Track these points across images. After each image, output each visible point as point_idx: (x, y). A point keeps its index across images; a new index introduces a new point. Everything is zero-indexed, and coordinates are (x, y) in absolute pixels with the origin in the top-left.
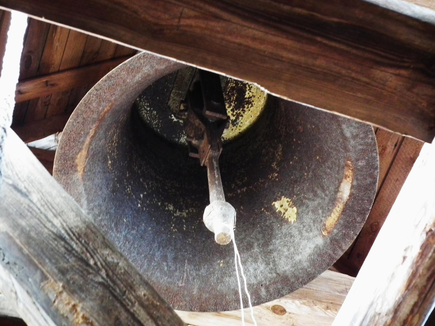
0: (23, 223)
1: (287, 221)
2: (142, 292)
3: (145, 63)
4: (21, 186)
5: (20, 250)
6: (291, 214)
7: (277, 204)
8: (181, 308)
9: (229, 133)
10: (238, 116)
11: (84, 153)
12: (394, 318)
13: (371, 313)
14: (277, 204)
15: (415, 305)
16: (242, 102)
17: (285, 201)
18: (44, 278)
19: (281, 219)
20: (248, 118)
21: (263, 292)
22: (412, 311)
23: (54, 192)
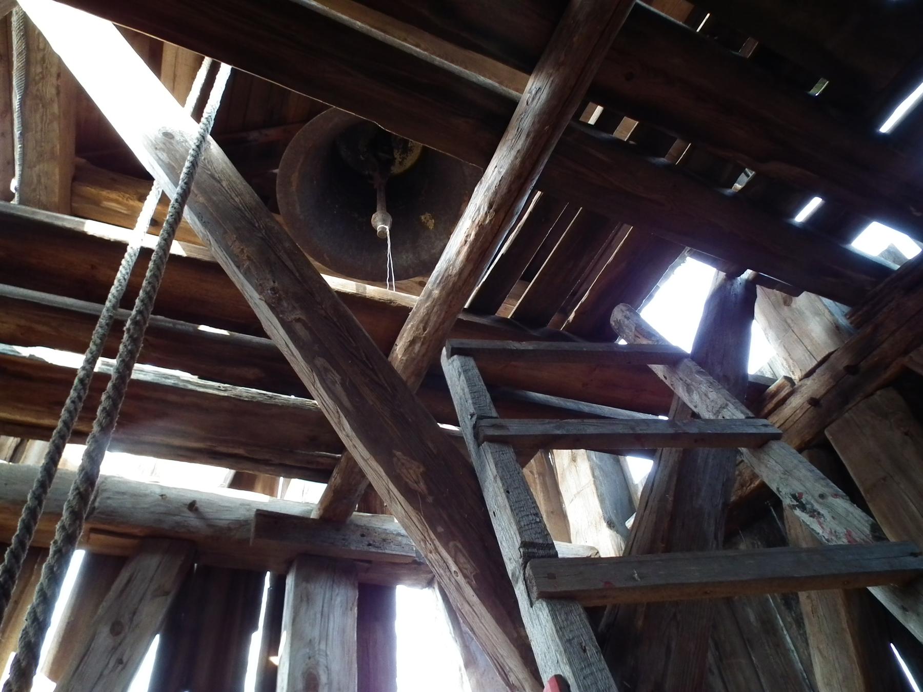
0: (215, 198)
1: (428, 228)
2: (287, 245)
3: (336, 115)
4: (216, 176)
5: (212, 214)
6: (431, 224)
7: (423, 217)
8: (190, 208)
9: (396, 169)
10: (403, 159)
11: (297, 174)
12: (459, 278)
13: (446, 275)
14: (423, 217)
15: (471, 271)
16: (406, 150)
17: (428, 215)
18: (225, 232)
19: (424, 227)
20: (410, 160)
21: (411, 271)
22: (469, 274)
23: (238, 181)
